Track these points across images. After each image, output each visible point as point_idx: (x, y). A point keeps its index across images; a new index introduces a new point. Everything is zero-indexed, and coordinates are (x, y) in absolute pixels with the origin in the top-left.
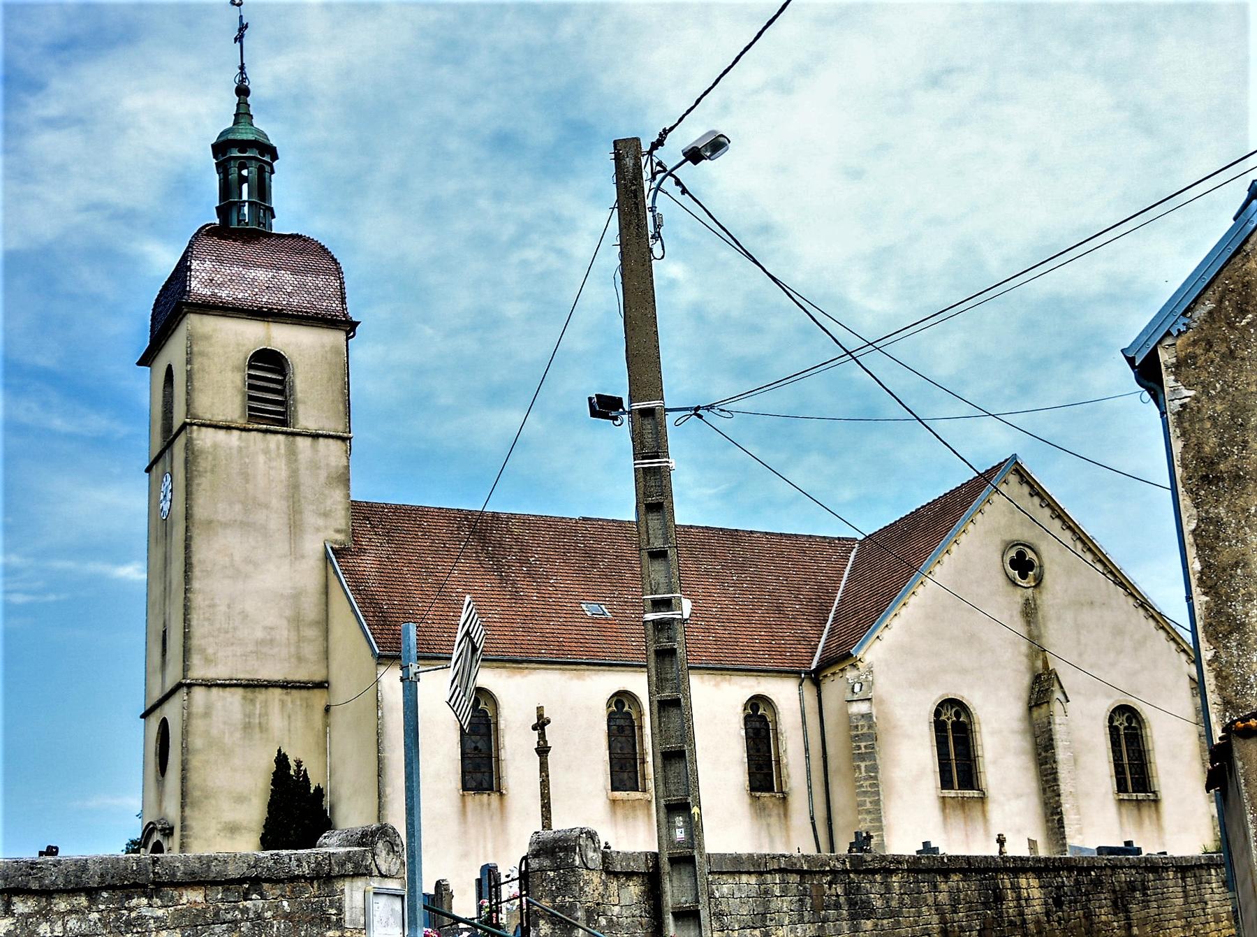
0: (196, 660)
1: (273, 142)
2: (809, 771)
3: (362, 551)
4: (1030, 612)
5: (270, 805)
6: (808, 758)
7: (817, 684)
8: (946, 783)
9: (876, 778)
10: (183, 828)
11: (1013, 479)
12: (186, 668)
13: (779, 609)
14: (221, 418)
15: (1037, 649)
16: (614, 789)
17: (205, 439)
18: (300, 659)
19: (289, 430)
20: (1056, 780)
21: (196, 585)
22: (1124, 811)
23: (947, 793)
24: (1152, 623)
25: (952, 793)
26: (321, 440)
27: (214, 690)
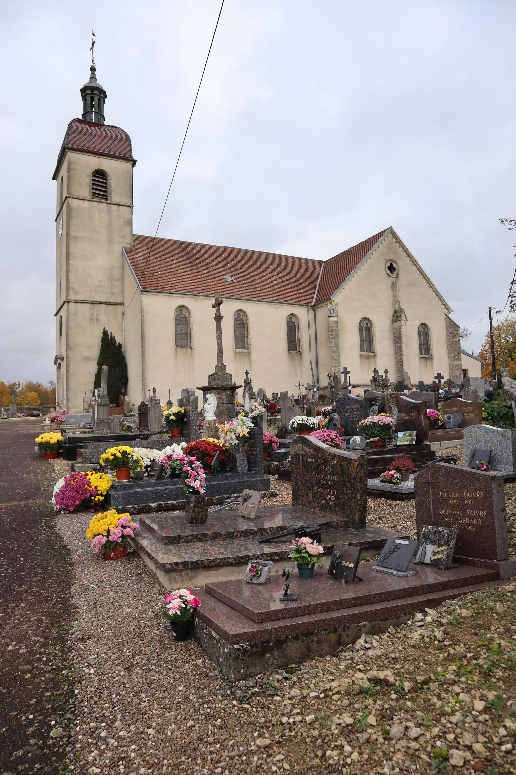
0: (71, 292)
1: (105, 89)
2: (310, 344)
3: (137, 252)
4: (394, 286)
5: (101, 350)
6: (310, 339)
7: (314, 310)
8: (362, 350)
9: (338, 347)
10: (67, 358)
11: (390, 236)
12: (67, 295)
13: (298, 283)
14: (81, 195)
15: (396, 301)
16: (236, 347)
17: (74, 203)
18: (113, 294)
19: (108, 202)
20: (401, 349)
21: (71, 262)
22: (421, 361)
23: (362, 353)
24: (434, 294)
25: (364, 353)
26: (121, 207)
27: (78, 304)
